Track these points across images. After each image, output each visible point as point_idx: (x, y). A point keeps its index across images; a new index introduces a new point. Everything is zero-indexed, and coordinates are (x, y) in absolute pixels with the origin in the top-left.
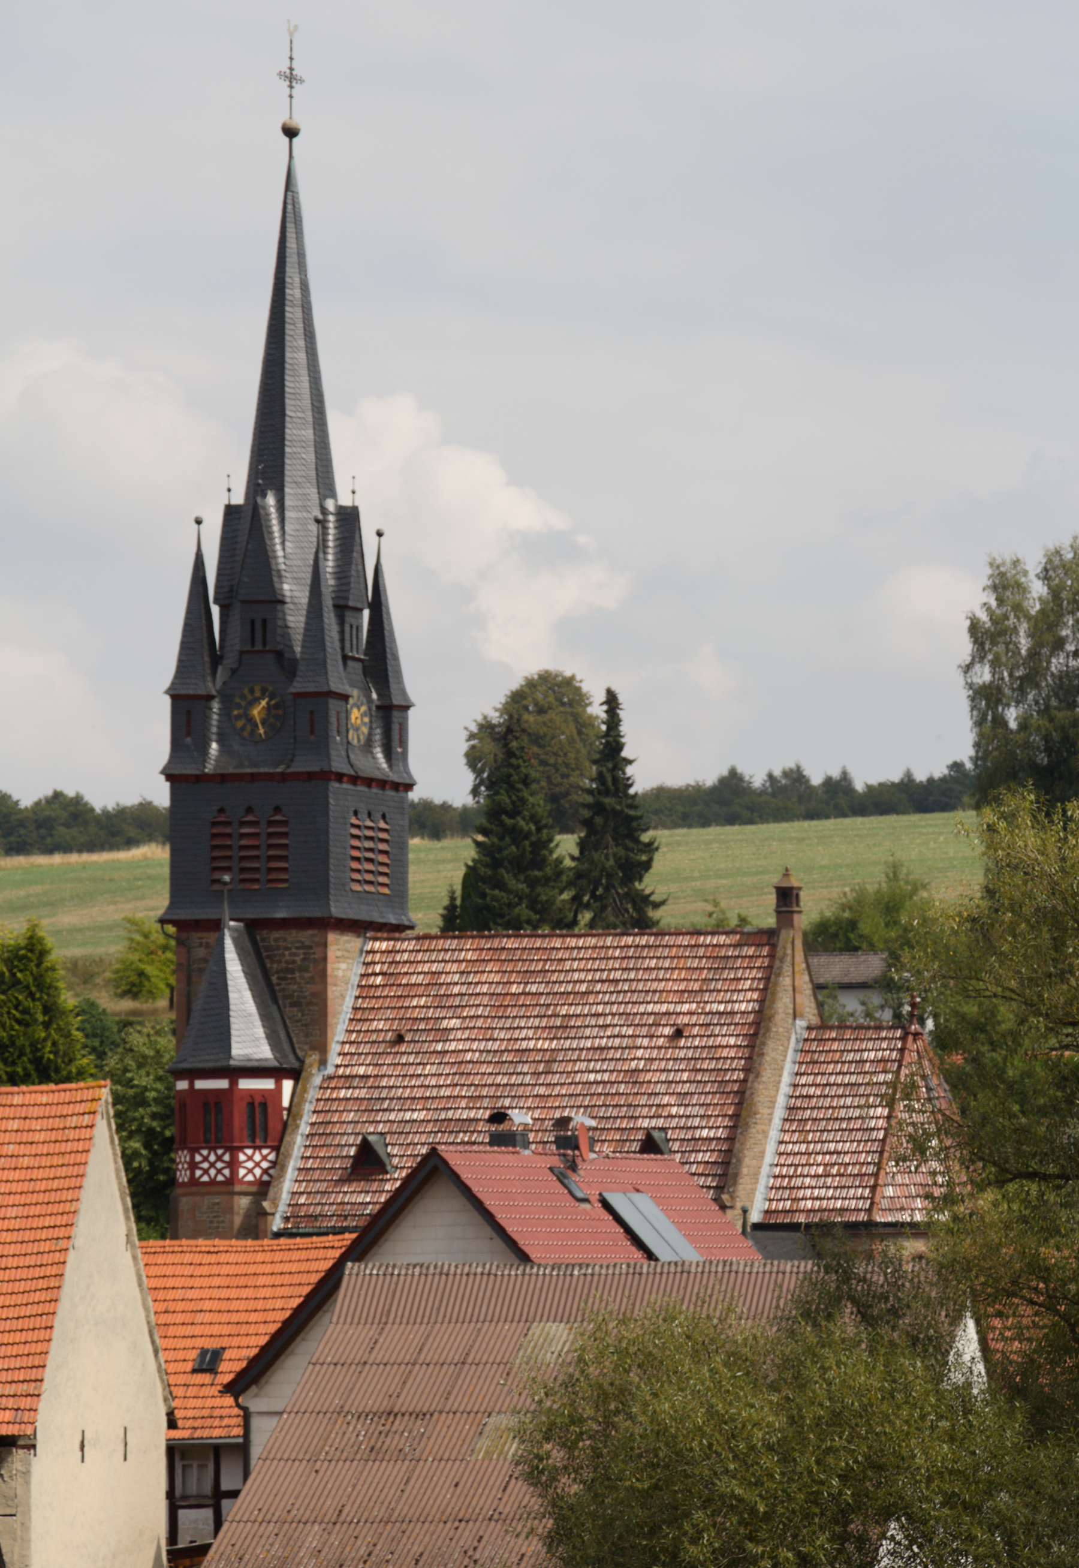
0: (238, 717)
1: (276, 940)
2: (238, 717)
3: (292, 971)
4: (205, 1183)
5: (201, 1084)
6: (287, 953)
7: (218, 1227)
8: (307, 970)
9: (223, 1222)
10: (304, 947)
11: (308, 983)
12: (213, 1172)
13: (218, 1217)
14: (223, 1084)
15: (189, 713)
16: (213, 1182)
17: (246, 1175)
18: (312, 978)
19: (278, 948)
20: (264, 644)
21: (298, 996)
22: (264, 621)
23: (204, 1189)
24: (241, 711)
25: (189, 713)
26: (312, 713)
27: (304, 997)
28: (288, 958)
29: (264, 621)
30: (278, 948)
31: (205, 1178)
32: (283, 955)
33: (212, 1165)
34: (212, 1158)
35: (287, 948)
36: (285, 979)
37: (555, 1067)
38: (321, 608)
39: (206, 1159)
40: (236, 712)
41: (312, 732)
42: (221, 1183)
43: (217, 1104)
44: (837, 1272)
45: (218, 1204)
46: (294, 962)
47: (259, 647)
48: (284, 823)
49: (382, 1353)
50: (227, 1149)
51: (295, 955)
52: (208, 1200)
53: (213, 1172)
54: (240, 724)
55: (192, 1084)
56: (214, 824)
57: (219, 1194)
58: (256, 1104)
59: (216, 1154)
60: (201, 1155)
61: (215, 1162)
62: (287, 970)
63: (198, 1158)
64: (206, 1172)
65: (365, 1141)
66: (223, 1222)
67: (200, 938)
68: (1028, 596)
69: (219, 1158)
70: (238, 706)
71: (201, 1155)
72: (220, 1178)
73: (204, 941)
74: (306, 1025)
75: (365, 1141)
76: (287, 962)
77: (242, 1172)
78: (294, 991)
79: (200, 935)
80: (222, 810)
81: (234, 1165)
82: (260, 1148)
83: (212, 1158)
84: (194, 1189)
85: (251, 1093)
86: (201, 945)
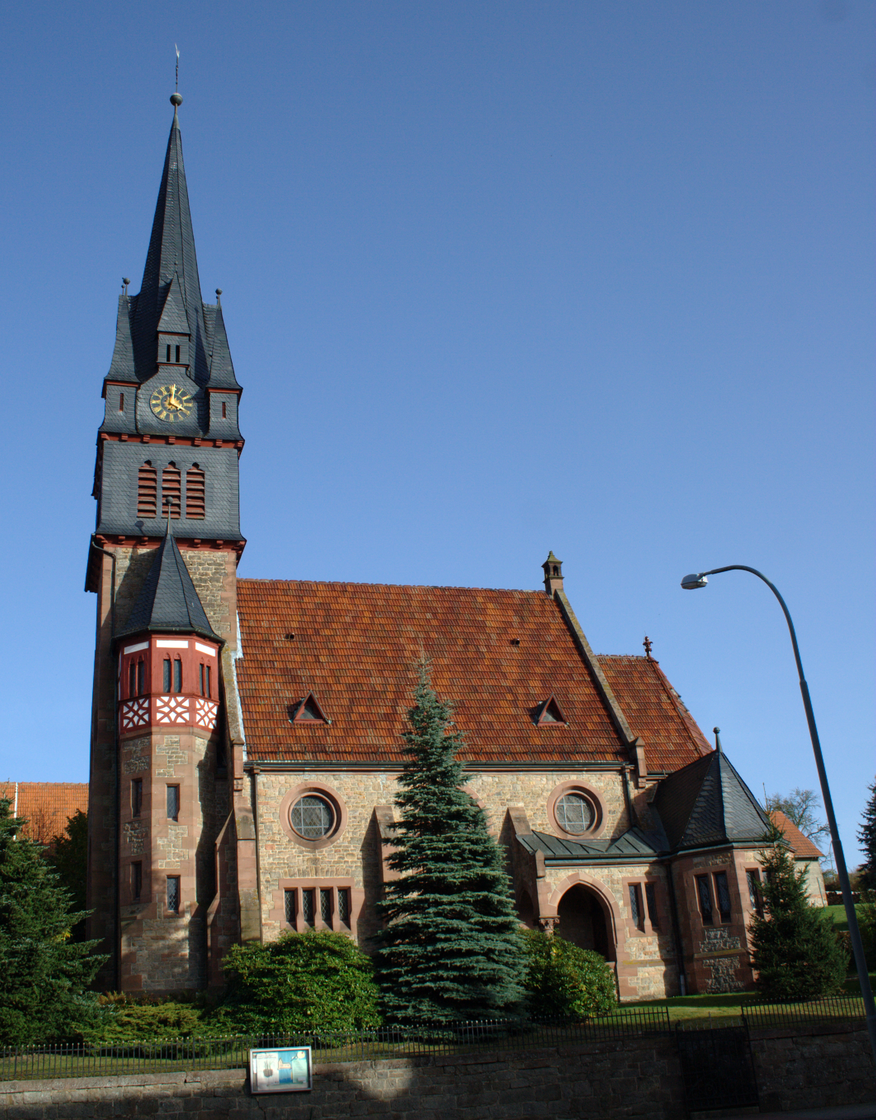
0: (156, 405)
1: (190, 557)
2: (156, 405)
4: (165, 724)
6: (201, 567)
7: (177, 762)
9: (181, 757)
16: (173, 724)
17: (162, 718)
20: (178, 359)
21: (211, 600)
23: (165, 730)
24: (158, 402)
28: (202, 571)
31: (166, 720)
32: (199, 569)
33: (172, 710)
35: (200, 564)
37: (832, 1008)
39: (167, 704)
40: (154, 402)
41: (224, 415)
42: (180, 725)
44: (312, 1033)
46: (206, 574)
47: (173, 359)
53: (173, 715)
57: (178, 733)
58: (172, 660)
59: (176, 701)
60: (162, 701)
61: (176, 707)
64: (166, 715)
68: (505, 863)
69: (179, 704)
71: (162, 701)
72: (180, 720)
77: (159, 716)
78: (207, 596)
81: (192, 710)
82: (175, 696)
83: (173, 704)
85: (168, 651)
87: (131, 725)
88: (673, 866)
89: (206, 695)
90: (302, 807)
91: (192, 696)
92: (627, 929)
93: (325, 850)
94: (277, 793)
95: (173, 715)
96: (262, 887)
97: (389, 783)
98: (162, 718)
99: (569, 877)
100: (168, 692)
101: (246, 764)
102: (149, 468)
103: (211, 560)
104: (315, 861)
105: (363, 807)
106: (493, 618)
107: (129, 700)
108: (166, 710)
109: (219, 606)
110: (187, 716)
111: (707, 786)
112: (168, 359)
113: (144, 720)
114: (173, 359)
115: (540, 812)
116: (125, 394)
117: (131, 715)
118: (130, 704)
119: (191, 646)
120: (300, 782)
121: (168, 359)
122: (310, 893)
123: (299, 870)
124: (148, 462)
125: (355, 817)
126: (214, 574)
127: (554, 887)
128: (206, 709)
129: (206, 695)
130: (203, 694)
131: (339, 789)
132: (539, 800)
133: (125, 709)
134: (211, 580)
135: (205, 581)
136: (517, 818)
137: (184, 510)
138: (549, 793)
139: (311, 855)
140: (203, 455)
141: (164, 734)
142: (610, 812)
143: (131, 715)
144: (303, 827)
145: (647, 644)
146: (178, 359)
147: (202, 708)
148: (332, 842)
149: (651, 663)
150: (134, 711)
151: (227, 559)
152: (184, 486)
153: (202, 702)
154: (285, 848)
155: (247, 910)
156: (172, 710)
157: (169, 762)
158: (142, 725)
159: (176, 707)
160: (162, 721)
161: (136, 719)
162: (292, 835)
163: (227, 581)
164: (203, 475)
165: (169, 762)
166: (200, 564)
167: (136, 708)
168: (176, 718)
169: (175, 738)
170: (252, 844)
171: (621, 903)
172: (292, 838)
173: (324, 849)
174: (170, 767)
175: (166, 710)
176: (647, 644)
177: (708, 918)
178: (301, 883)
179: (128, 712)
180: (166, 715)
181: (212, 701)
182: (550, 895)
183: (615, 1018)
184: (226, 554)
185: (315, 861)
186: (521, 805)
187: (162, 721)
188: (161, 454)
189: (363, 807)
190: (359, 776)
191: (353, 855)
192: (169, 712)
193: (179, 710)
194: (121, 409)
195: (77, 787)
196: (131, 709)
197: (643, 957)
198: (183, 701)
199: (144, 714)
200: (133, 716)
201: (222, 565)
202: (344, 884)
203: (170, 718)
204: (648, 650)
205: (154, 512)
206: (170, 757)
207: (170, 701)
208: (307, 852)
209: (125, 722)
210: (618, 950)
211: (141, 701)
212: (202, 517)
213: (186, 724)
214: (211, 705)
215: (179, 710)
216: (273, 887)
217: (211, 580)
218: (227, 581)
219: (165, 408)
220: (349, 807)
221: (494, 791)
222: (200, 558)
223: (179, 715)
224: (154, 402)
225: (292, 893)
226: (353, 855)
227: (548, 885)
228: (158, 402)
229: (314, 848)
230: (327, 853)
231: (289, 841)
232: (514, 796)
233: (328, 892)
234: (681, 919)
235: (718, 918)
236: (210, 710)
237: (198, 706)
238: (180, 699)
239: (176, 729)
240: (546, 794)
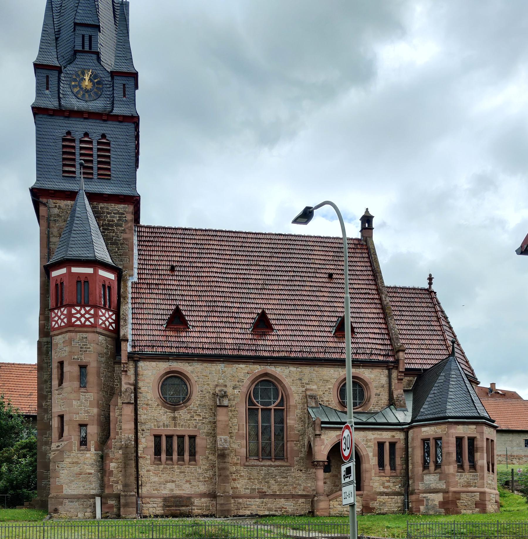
0: (75, 86)
1: (101, 208)
2: (75, 86)
3: (112, 226)
4: (78, 326)
5: (74, 270)
6: (109, 216)
11: (121, 233)
12: (83, 320)
13: (86, 345)
15: (47, 77)
16: (83, 325)
18: (124, 230)
19: (103, 213)
20: (90, 47)
21: (116, 240)
23: (77, 329)
24: (77, 83)
25: (47, 77)
26: (124, 85)
27: (119, 240)
28: (109, 218)
29: (90, 37)
30: (103, 213)
31: (78, 323)
33: (83, 316)
35: (108, 213)
36: (108, 229)
40: (73, 83)
41: (124, 96)
43: (86, 282)
45: (86, 338)
46: (113, 221)
52: (79, 335)
53: (83, 320)
54: (75, 90)
55: (69, 271)
57: (86, 332)
58: (107, 286)
59: (85, 310)
60: (76, 310)
62: (109, 225)
63: (74, 311)
64: (79, 319)
65: (177, 307)
66: (90, 348)
67: (54, 203)
69: (87, 312)
71: (76, 310)
72: (88, 323)
73: (57, 205)
74: (120, 255)
75: (177, 307)
79: (55, 201)
80: (69, 133)
81: (96, 316)
83: (83, 312)
89: (107, 307)
91: (95, 307)
92: (373, 471)
93: (182, 412)
95: (62, 317)
96: (139, 434)
99: (337, 436)
100: (104, 308)
101: (129, 353)
102: (68, 138)
103: (116, 210)
104: (174, 418)
105: (208, 384)
106: (318, 255)
107: (55, 309)
108: (78, 316)
109: (122, 244)
112: (83, 48)
116: (50, 76)
118: (56, 311)
119: (96, 272)
121: (83, 48)
123: (164, 424)
124: (104, 136)
125: (202, 391)
127: (326, 442)
128: (107, 316)
129: (107, 307)
131: (192, 372)
138: (335, 380)
139: (172, 415)
145: (430, 279)
146: (90, 47)
147: (104, 315)
149: (429, 292)
153: (104, 311)
159: (85, 314)
160: (66, 322)
161: (59, 321)
162: (158, 402)
163: (127, 226)
164: (108, 144)
166: (108, 213)
168: (85, 322)
171: (371, 454)
172: (160, 403)
173: (181, 411)
175: (78, 316)
176: (430, 279)
177: (425, 466)
178: (164, 432)
180: (79, 319)
182: (323, 447)
184: (126, 206)
185: (174, 418)
186: (314, 387)
187: (66, 322)
188: (79, 128)
192: (81, 317)
194: (124, 96)
196: (56, 315)
197: (382, 490)
198: (90, 310)
200: (58, 320)
201: (124, 214)
202: (192, 434)
204: (430, 284)
205: (74, 172)
206: (81, 348)
209: (54, 323)
211: (62, 309)
212: (91, 176)
213: (93, 326)
214: (111, 313)
216: (147, 434)
218: (127, 226)
219: (81, 88)
221: (297, 377)
223: (87, 319)
224: (73, 83)
225: (157, 438)
228: (77, 83)
229: (174, 410)
230: (183, 414)
231: (158, 405)
232: (311, 381)
233: (181, 438)
234: (410, 467)
235: (432, 467)
236: (110, 317)
237: (100, 314)
239: (85, 329)
240: (334, 381)
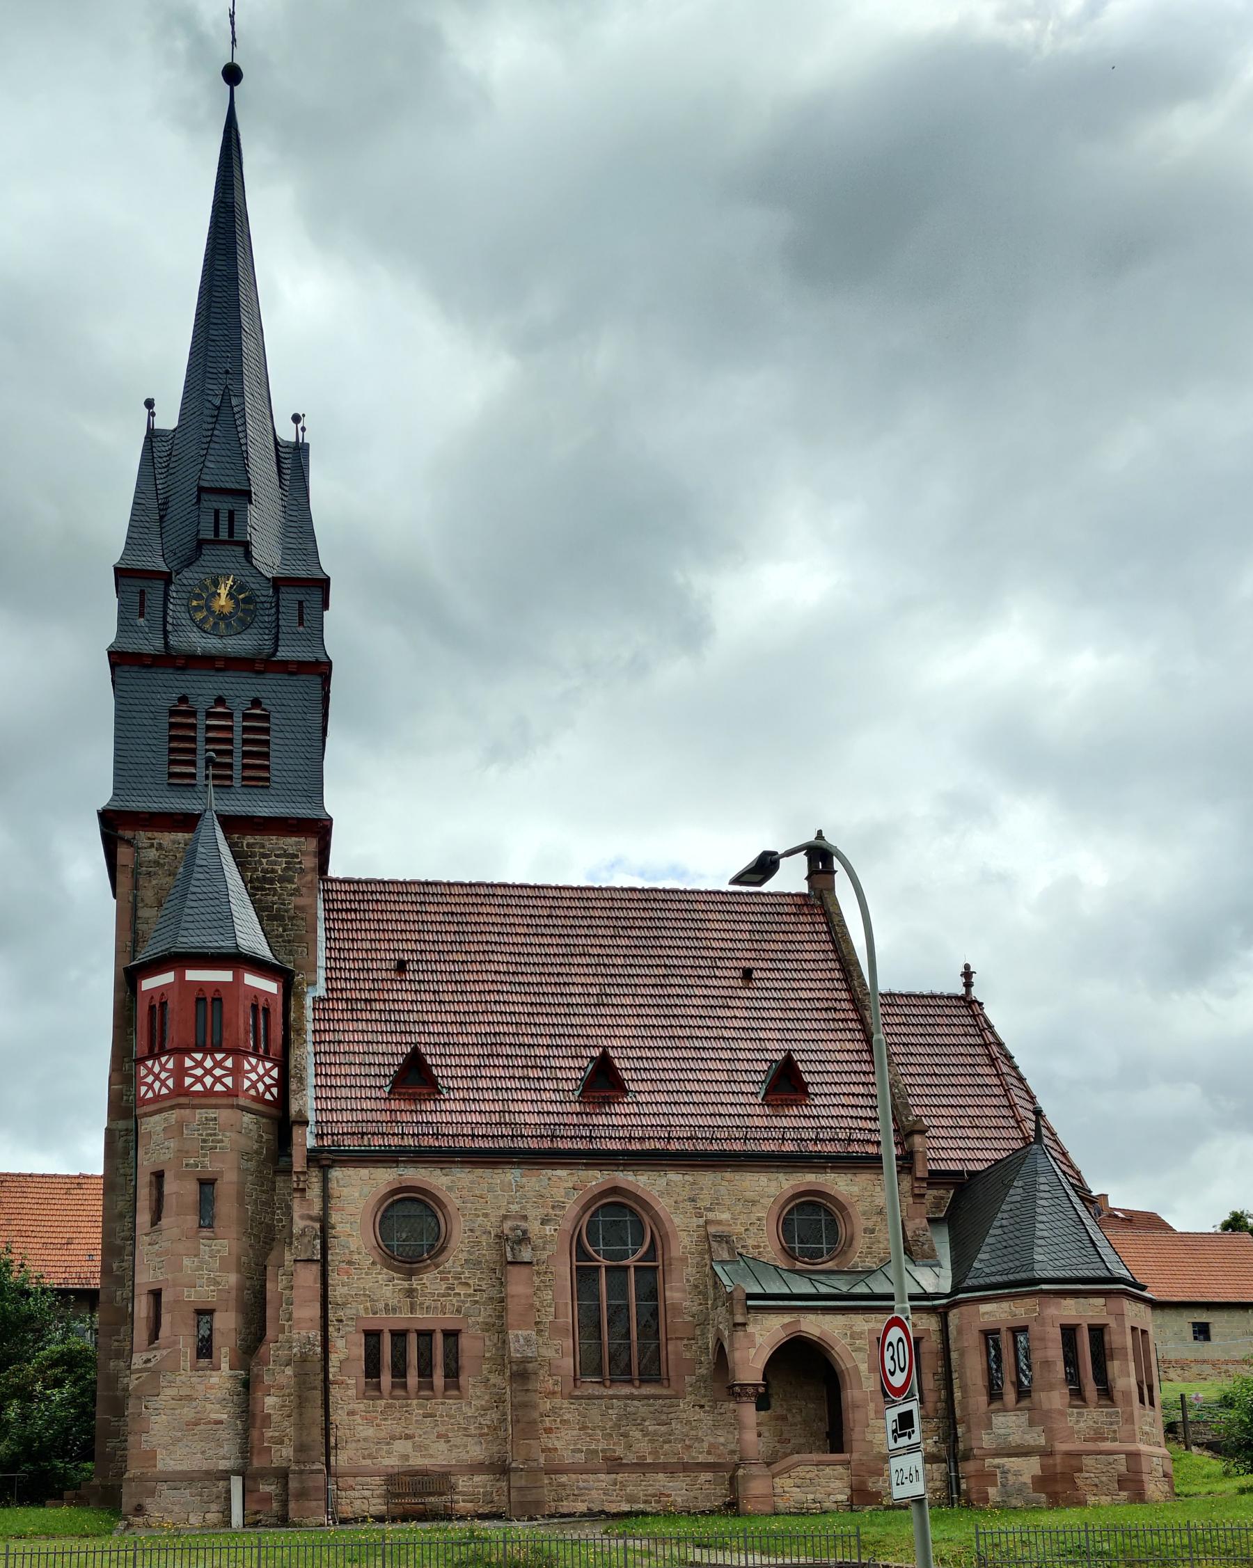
1: (248, 845)
3: (272, 881)
5: (192, 975)
6: (264, 861)
8: (291, 881)
9: (222, 1141)
10: (285, 855)
11: (291, 895)
13: (215, 1135)
14: (226, 976)
15: (142, 593)
16: (209, 1093)
17: (192, 1085)
19: (253, 855)
20: (231, 533)
21: (279, 910)
22: (231, 514)
23: (196, 1101)
24: (202, 603)
25: (142, 593)
29: (231, 514)
30: (253, 855)
31: (198, 1087)
33: (208, 1072)
34: (209, 1063)
35: (264, 856)
36: (264, 889)
38: (123, 653)
40: (195, 603)
41: (301, 623)
46: (273, 871)
47: (224, 535)
48: (266, 718)
49: (979, 1070)
50: (229, 1052)
51: (275, 863)
52: (200, 1114)
53: (208, 1080)
54: (199, 616)
56: (173, 713)
57: (216, 1107)
59: (214, 1059)
60: (193, 1059)
62: (264, 880)
64: (199, 1079)
66: (222, 1141)
69: (218, 1064)
70: (199, 597)
71: (193, 1059)
72: (219, 1087)
73: (155, 842)
74: (289, 941)
76: (265, 871)
79: (149, 834)
81: (237, 1072)
83: (209, 1063)
84: (183, 1100)
86: (152, 845)
87: (150, 1095)
88: (951, 1314)
89: (261, 1052)
90: (795, 1217)
91: (237, 1052)
93: (427, 1278)
94: (357, 1194)
95: (163, 1075)
97: (524, 1180)
98: (192, 1085)
99: (784, 1326)
102: (182, 711)
104: (410, 1293)
105: (486, 1215)
107: (148, 1058)
108: (199, 1072)
110: (228, 1081)
111: (1015, 1194)
112: (217, 534)
113: (167, 1087)
114: (224, 535)
115: (753, 1229)
117: (150, 1079)
118: (150, 1063)
120: (391, 1178)
121: (217, 534)
122: (399, 1336)
123: (387, 1305)
125: (472, 1231)
126: (284, 870)
128: (261, 1071)
129: (261, 1052)
130: (256, 1047)
131: (450, 1189)
132: (754, 1209)
133: (143, 1072)
134: (282, 879)
135: (272, 881)
136: (715, 1236)
137: (237, 773)
139: (406, 1284)
140: (269, 688)
141: (195, 1107)
142: (865, 1231)
143: (150, 1079)
144: (797, 1245)
146: (231, 533)
148: (437, 1266)
149: (968, 1003)
150: (154, 1074)
151: (304, 848)
152: (238, 736)
153: (254, 1061)
154: (367, 1274)
155: (1184, 1339)
156: (208, 1072)
157: (202, 1148)
158: (197, 1092)
161: (157, 1085)
164: (266, 718)
165: (202, 1148)
166: (264, 856)
167: (157, 1069)
168: (213, 1085)
169: (212, 1113)
170: (315, 1269)
171: (863, 1367)
172: (377, 1259)
173: (425, 1276)
174: (205, 1156)
177: (994, 1394)
178: (387, 1323)
179: (146, 1076)
180: (199, 1079)
181: (270, 1060)
182: (752, 1351)
183: (554, 1545)
184: (303, 839)
185: (410, 1293)
186: (725, 1216)
188: (203, 689)
189: (486, 1215)
190: (487, 1172)
191: (467, 1284)
192: (204, 1076)
193: (218, 1072)
195: (80, 1181)
196: (150, 1071)
198: (224, 1059)
199: (167, 1078)
201: (297, 856)
203: (204, 1085)
204: (968, 985)
205: (193, 776)
206: (204, 1141)
207: (204, 1059)
208: (399, 1279)
209: (143, 1089)
210: (856, 1435)
211: (163, 1059)
213: (231, 1093)
214: (268, 1065)
215: (218, 1072)
217: (282, 879)
220: (464, 1216)
222: (263, 847)
223: (218, 1080)
224: (195, 603)
225: (372, 1337)
226: (467, 1284)
227: (750, 1337)
228: (202, 603)
229: (410, 1274)
230: (429, 1282)
231: (374, 1263)
232: (716, 1204)
234: (957, 1395)
235: (1010, 1395)
237: (247, 1067)
238: (219, 1056)
239: (213, 1101)
